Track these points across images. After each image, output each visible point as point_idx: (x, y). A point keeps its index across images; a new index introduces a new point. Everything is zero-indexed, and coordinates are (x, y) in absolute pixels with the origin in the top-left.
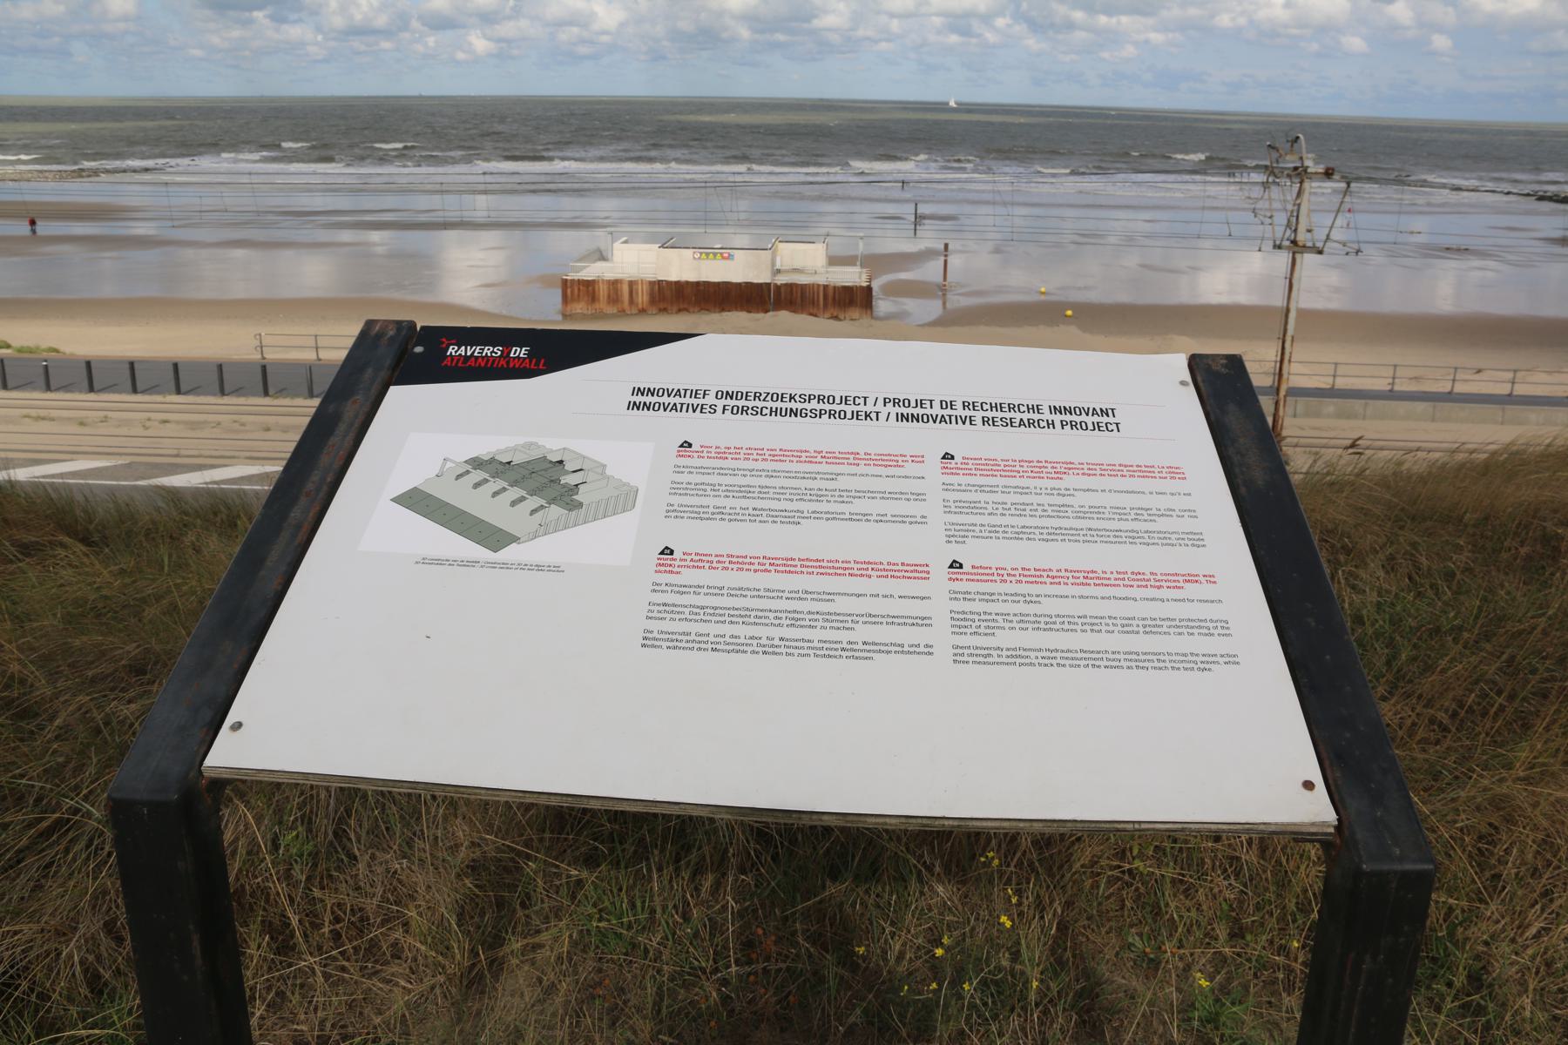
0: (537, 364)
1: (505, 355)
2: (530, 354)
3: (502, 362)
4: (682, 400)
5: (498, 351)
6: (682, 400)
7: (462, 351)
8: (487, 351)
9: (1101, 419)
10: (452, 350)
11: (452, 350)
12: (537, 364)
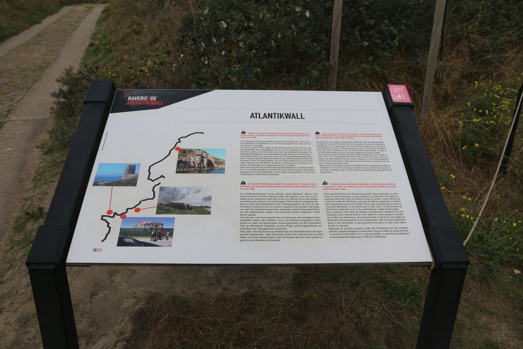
1: (148, 100)
2: (157, 99)
5: (146, 98)
7: (142, 98)
8: (142, 98)
11: (129, 98)
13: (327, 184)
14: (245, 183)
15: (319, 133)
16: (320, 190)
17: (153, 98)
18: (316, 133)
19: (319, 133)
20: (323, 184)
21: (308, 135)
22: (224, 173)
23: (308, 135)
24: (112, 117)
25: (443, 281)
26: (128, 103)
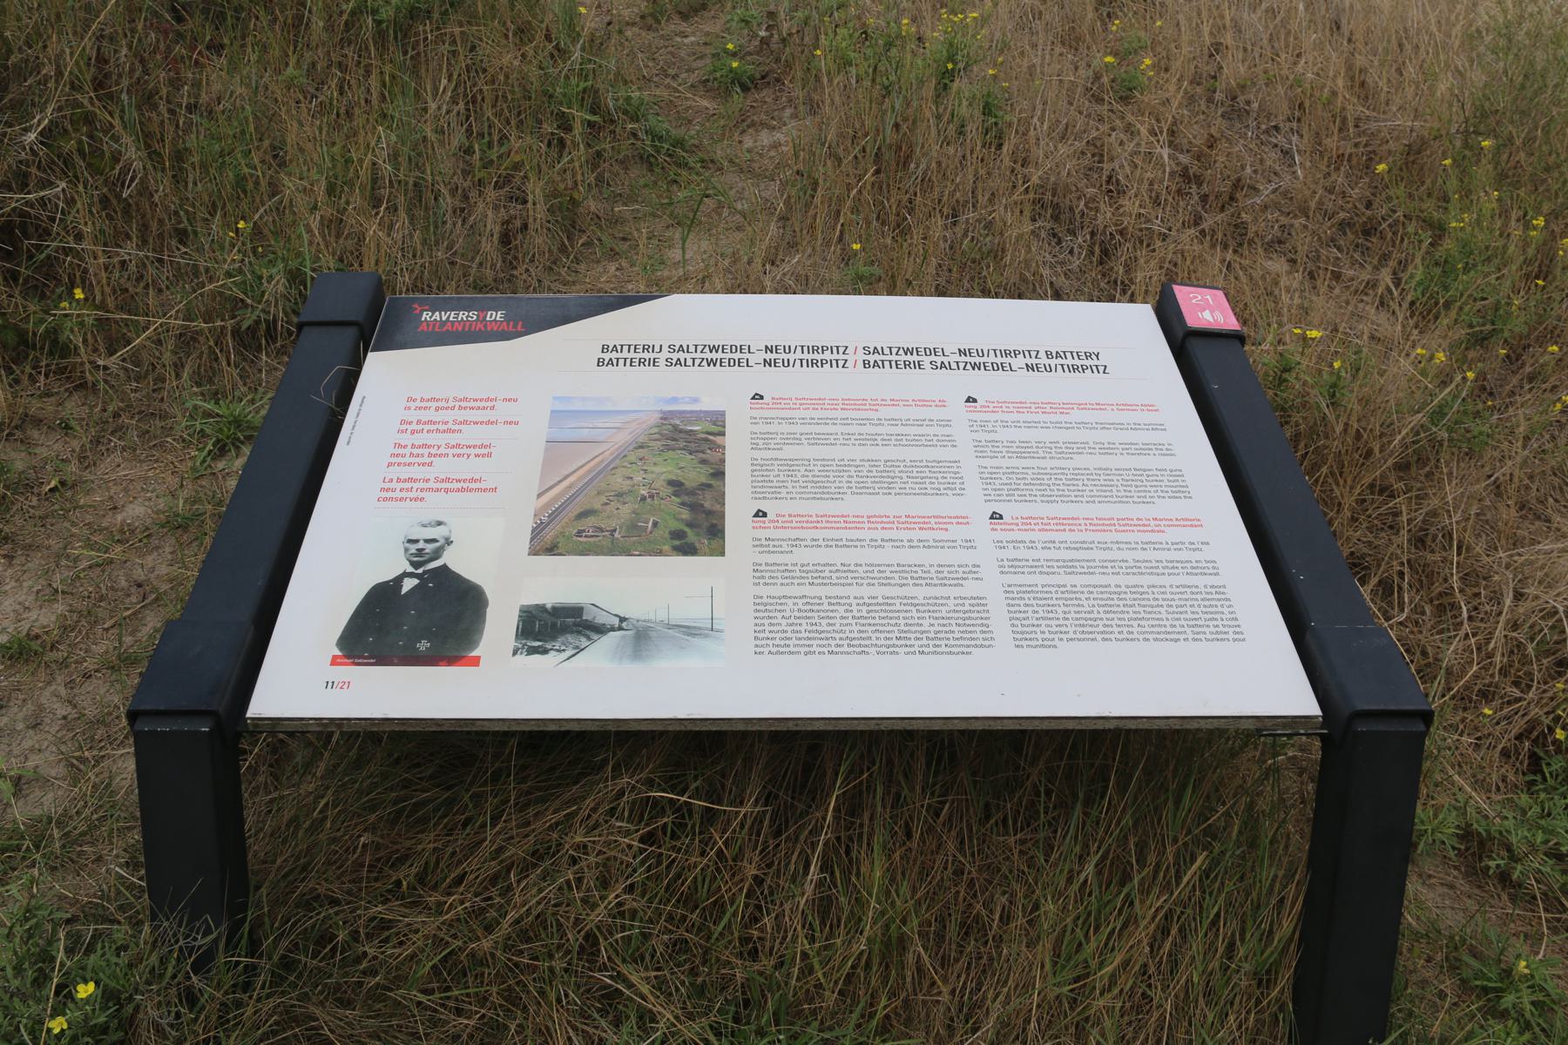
3: (480, 326)
4: (619, 355)
5: (473, 315)
6: (619, 355)
8: (462, 315)
11: (426, 316)
21: (942, 404)
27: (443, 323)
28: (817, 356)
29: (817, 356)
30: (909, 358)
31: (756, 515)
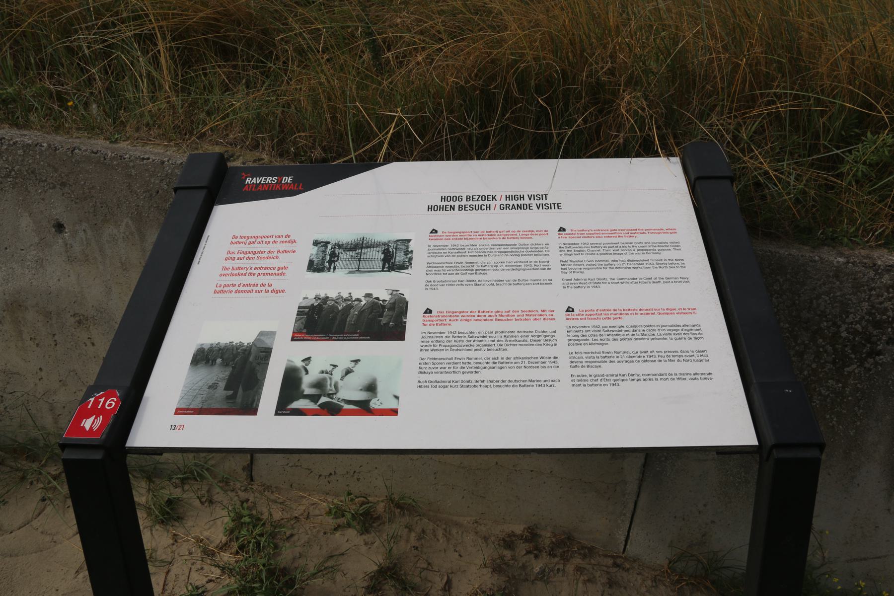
0: (298, 187)
1: (279, 182)
2: (293, 181)
3: (278, 187)
8: (269, 180)
9: (541, 201)
10: (248, 181)
11: (248, 181)
12: (298, 187)
13: (573, 310)
14: (431, 312)
15: (564, 230)
16: (554, 240)
17: (287, 180)
18: (560, 230)
19: (564, 230)
20: (567, 311)
21: (545, 233)
22: (403, 339)
23: (545, 233)
24: (649, 196)
25: (780, 474)
26: (246, 188)
27: (257, 185)
28: (479, 203)
29: (479, 203)
30: (516, 203)
31: (426, 312)
